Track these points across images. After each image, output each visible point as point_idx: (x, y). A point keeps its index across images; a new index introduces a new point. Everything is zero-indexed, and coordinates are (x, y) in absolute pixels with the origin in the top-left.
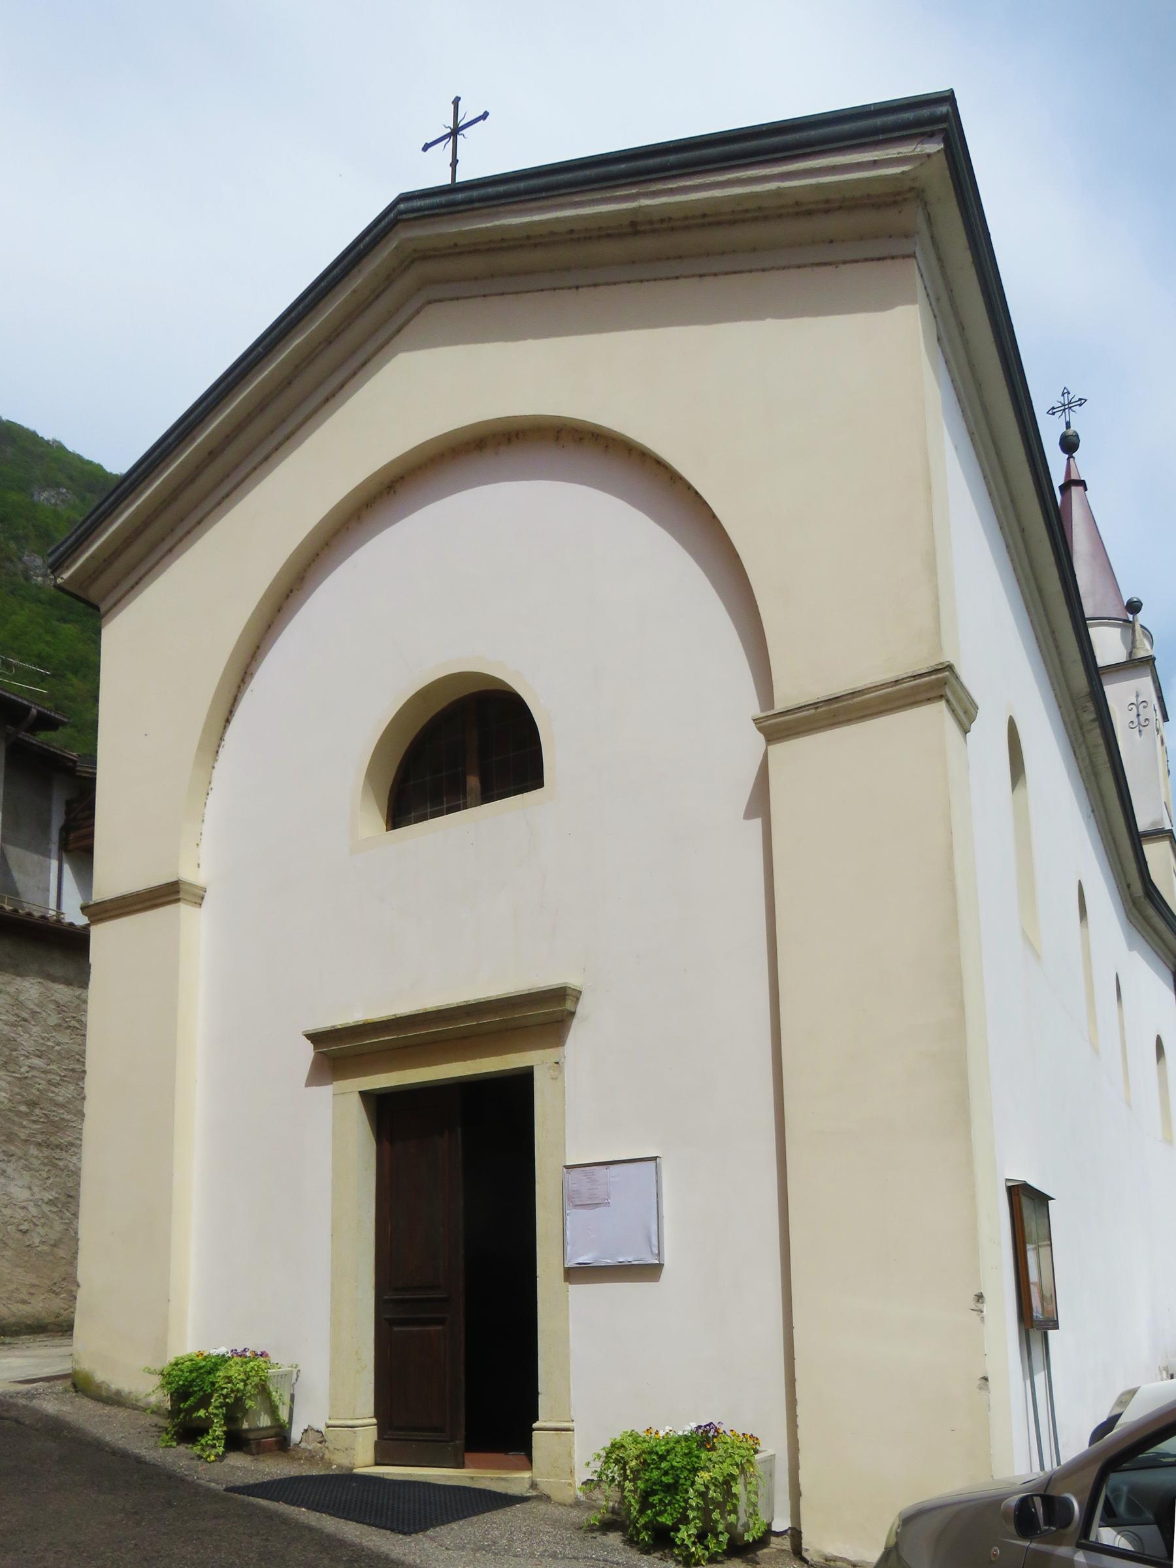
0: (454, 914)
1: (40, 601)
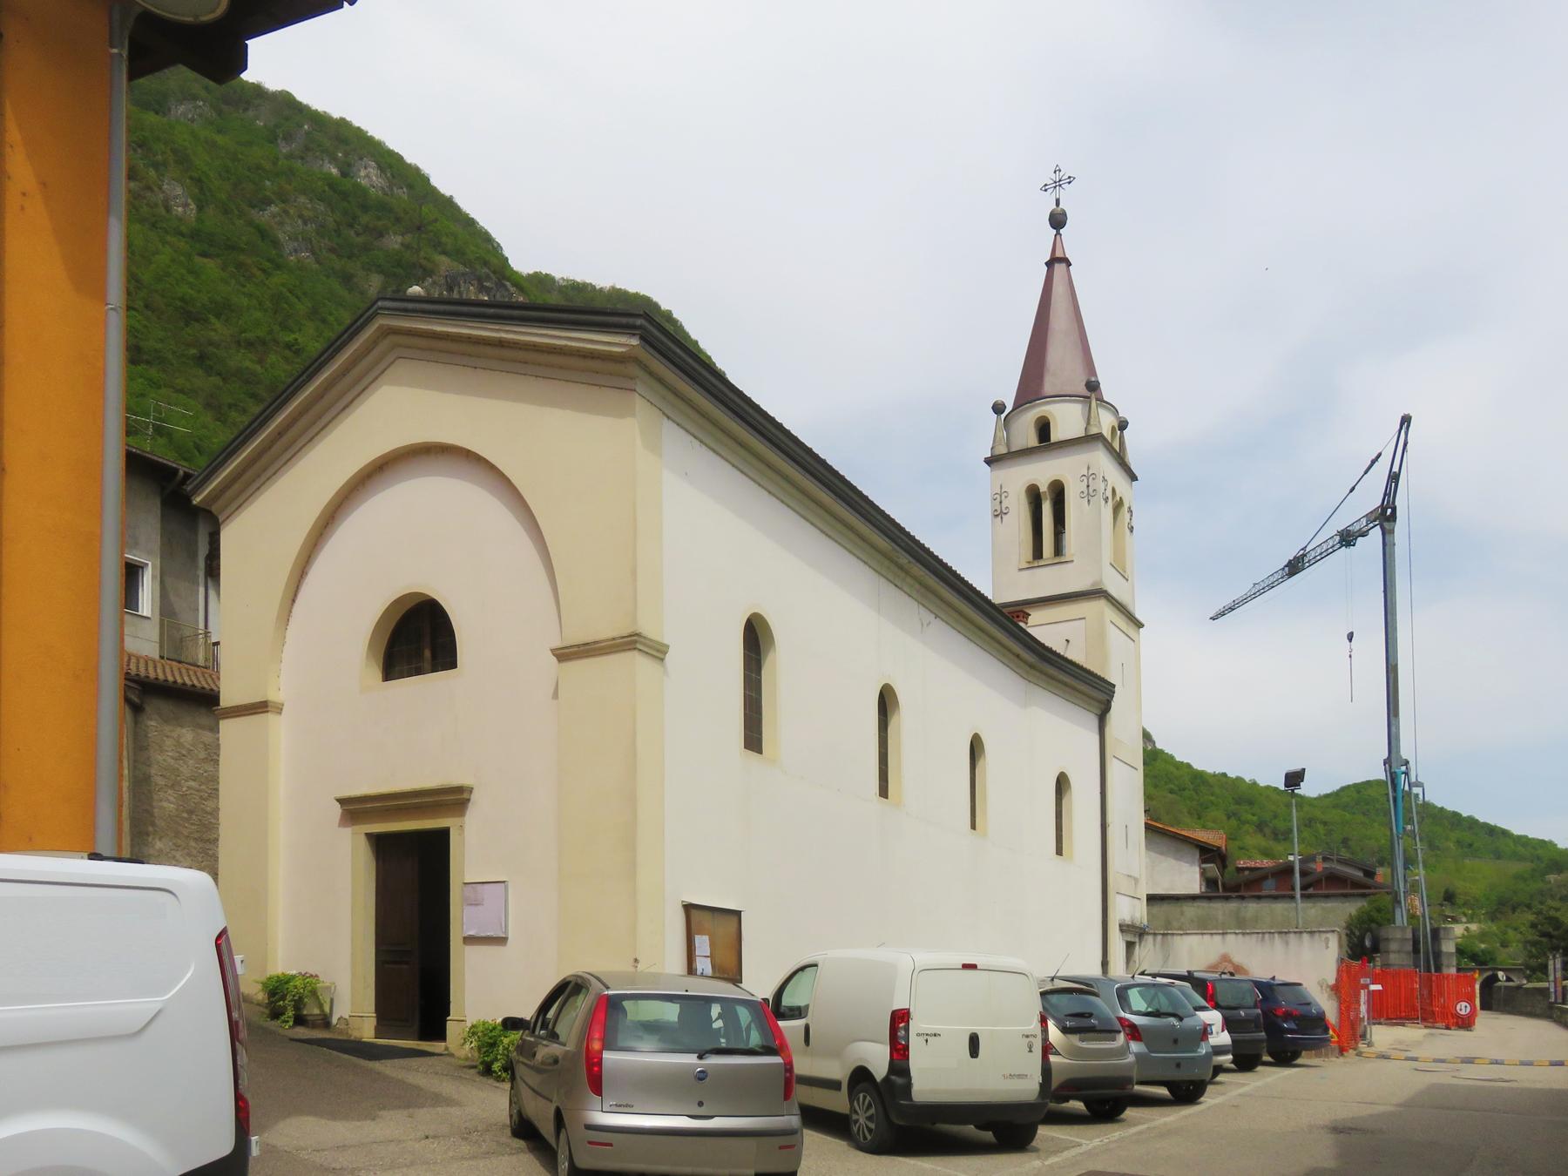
0: (413, 737)
1: (182, 235)
